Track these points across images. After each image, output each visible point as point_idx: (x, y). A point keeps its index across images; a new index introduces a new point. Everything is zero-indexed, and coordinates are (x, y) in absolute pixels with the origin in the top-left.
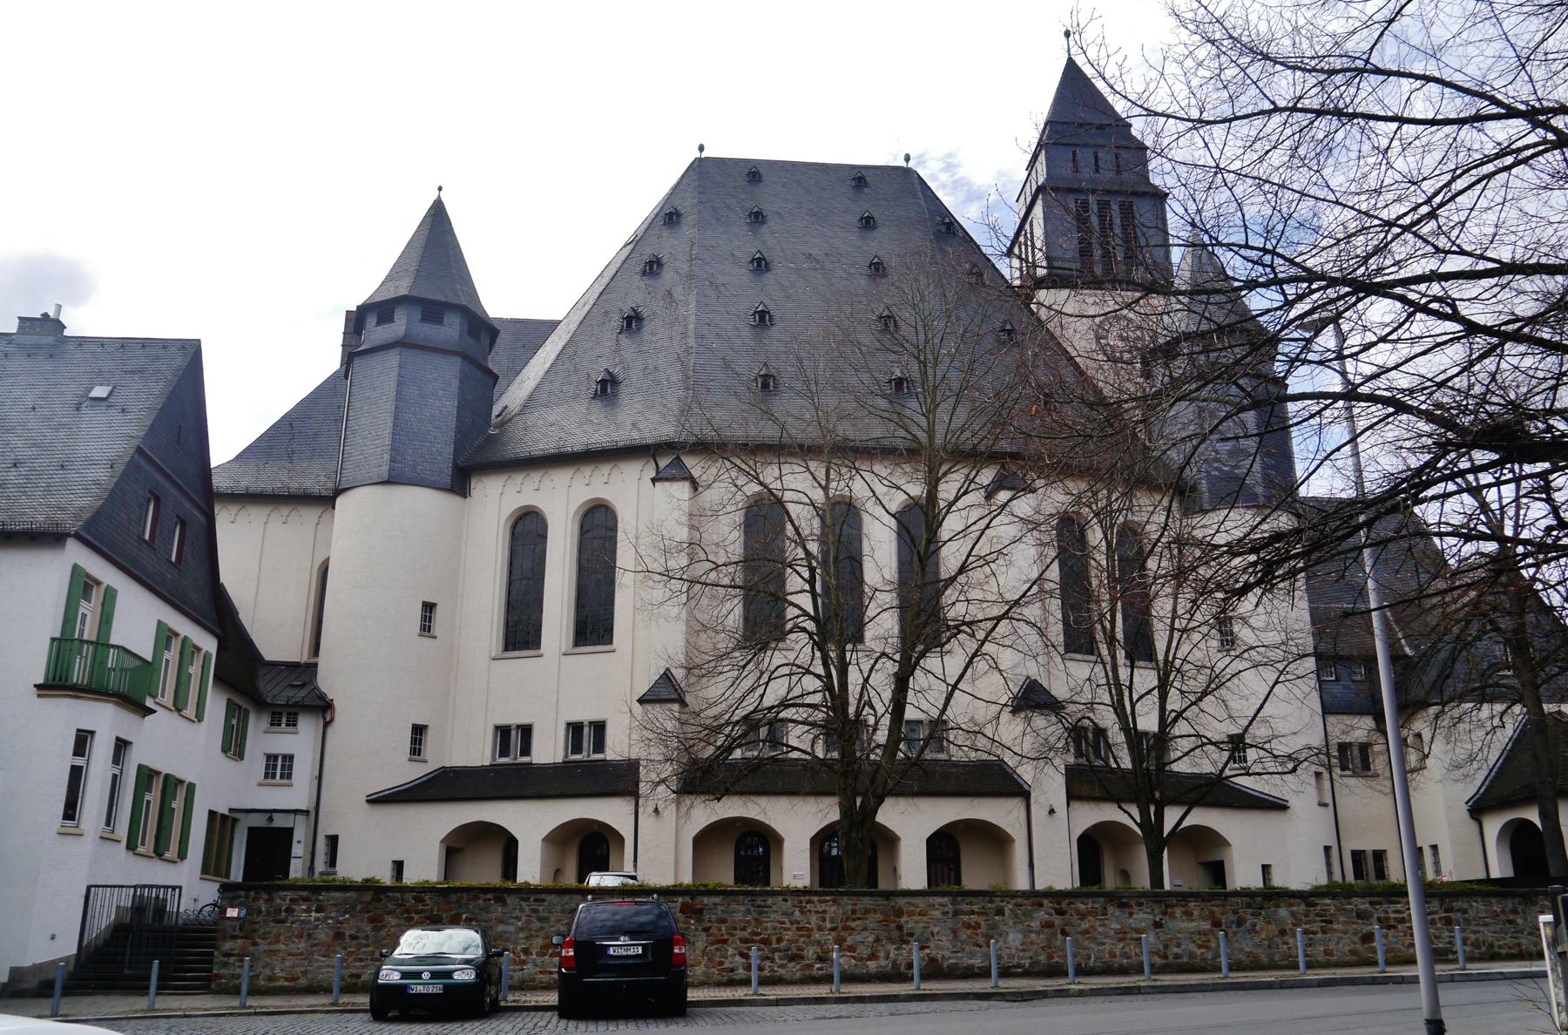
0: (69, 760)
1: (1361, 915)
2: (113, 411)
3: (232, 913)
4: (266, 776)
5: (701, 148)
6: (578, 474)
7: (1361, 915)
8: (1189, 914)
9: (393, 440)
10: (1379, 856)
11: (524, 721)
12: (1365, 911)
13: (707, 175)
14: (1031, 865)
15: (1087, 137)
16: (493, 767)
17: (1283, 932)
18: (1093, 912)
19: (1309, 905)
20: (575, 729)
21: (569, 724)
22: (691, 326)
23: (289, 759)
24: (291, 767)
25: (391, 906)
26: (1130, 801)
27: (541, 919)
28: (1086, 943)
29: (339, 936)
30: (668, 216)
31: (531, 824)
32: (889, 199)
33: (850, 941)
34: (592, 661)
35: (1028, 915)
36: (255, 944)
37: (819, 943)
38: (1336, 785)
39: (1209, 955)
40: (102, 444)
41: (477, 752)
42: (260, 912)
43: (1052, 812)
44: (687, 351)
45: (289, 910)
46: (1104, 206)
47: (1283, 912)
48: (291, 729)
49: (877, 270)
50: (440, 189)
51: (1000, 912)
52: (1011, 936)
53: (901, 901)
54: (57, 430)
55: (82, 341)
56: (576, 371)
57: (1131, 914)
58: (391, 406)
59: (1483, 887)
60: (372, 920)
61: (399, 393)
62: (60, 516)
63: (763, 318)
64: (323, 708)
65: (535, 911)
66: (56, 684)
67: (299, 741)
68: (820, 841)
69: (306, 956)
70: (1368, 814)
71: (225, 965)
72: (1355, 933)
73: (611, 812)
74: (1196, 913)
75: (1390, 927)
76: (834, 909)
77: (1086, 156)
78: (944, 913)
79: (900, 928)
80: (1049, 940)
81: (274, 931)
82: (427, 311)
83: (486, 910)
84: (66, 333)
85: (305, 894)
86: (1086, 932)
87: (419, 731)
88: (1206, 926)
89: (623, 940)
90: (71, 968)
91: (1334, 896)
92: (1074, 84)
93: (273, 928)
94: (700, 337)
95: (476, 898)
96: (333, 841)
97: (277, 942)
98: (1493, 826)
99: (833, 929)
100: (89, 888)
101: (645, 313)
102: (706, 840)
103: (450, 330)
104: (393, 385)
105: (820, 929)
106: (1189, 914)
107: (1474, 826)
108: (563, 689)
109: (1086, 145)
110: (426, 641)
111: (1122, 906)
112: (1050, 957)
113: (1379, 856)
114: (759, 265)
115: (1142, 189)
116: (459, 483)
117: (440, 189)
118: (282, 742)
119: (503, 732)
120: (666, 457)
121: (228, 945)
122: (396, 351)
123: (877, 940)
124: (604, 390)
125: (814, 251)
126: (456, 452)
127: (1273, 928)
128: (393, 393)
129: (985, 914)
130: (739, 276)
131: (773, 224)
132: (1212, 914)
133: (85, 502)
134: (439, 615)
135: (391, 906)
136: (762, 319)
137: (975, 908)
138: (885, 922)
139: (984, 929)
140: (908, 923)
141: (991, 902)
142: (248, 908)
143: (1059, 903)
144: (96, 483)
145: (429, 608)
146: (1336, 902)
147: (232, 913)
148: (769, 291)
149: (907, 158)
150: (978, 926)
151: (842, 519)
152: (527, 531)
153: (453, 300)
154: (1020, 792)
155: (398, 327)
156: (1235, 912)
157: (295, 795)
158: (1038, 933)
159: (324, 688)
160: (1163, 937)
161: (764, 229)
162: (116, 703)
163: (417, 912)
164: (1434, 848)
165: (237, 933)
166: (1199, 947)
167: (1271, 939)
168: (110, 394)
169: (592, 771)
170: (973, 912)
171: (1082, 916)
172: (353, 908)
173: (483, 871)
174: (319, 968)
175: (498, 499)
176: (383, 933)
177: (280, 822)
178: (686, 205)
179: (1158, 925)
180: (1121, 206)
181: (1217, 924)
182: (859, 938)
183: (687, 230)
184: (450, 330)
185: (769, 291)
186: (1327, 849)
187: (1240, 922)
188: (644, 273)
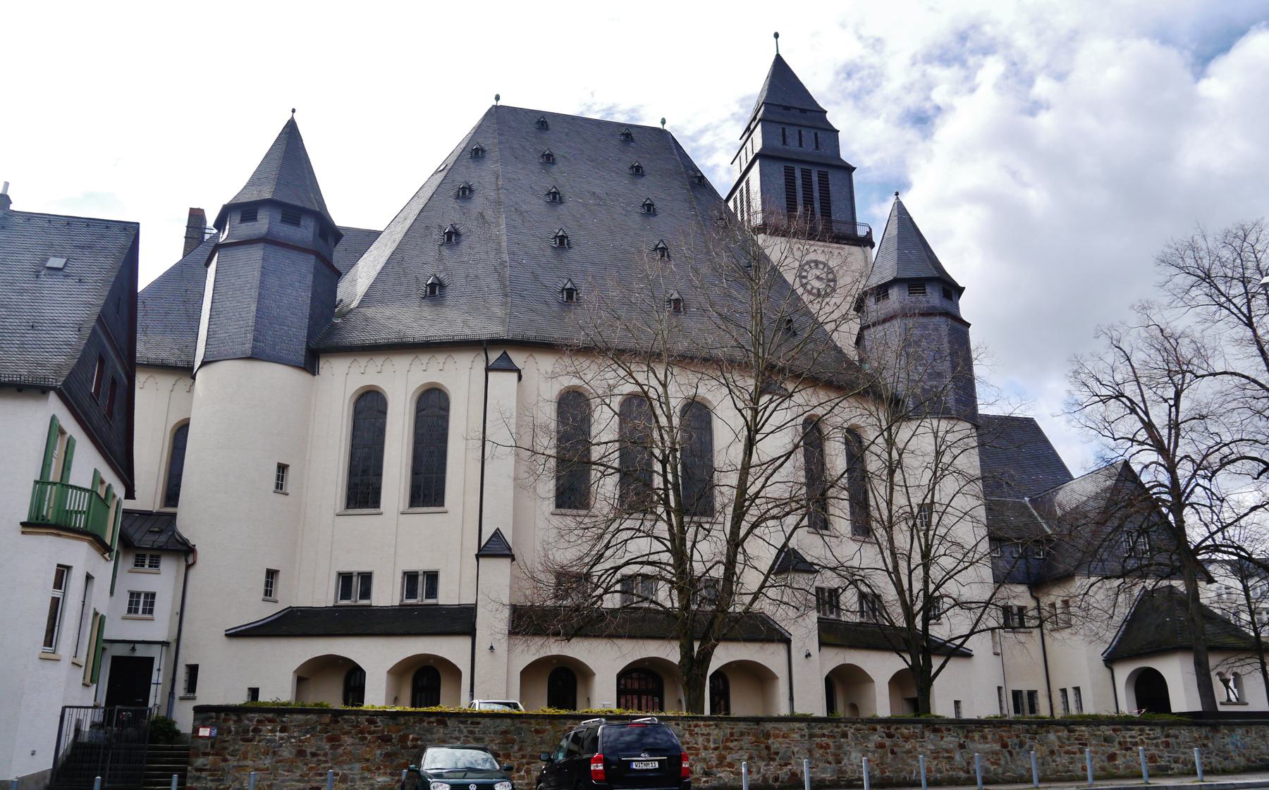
0: (52, 592)
1: (1107, 740)
2: (70, 281)
3: (204, 732)
4: (130, 611)
5: (497, 98)
6: (417, 362)
7: (1107, 740)
8: (984, 737)
9: (257, 323)
10: (1032, 694)
11: (365, 569)
12: (1110, 736)
13: (502, 119)
14: (791, 699)
15: (791, 119)
16: (336, 608)
17: (1052, 752)
18: (914, 736)
19: (1070, 731)
20: (411, 578)
21: (340, 574)
22: (504, 244)
23: (151, 596)
24: (152, 604)
25: (347, 727)
26: (904, 651)
28: (910, 761)
29: (301, 753)
30: (473, 151)
31: (378, 658)
32: (648, 154)
33: (729, 759)
34: (426, 520)
35: (866, 738)
36: (225, 760)
37: (704, 760)
38: (1046, 638)
39: (1000, 770)
40: (68, 311)
41: (323, 595)
42: (230, 732)
43: (808, 655)
44: (503, 264)
45: (256, 730)
47: (1052, 737)
48: (153, 570)
49: (649, 210)
50: (294, 111)
51: (845, 735)
52: (853, 755)
53: (769, 726)
54: (21, 294)
55: (29, 217)
56: (405, 275)
57: (942, 738)
58: (254, 293)
59: (1184, 719)
60: (330, 739)
61: (262, 282)
62: (41, 372)
63: (562, 242)
64: (185, 551)
65: (471, 732)
66: (35, 524)
67: (162, 580)
69: (272, 771)
71: (198, 779)
72: (1103, 754)
74: (990, 737)
75: (1127, 749)
76: (716, 732)
77: (792, 132)
78: (803, 736)
79: (768, 748)
80: (881, 758)
81: (243, 749)
82: (283, 209)
84: (12, 207)
85: (270, 716)
86: (909, 752)
87: (271, 574)
88: (997, 747)
89: (644, 756)
90: (47, 781)
91: (1087, 724)
92: (781, 73)
93: (241, 746)
94: (511, 253)
95: (421, 721)
96: (193, 670)
97: (245, 758)
98: (1123, 672)
99: (716, 749)
100: (64, 708)
101: (462, 230)
102: (529, 674)
103: (305, 232)
104: (257, 274)
105: (706, 748)
106: (984, 737)
107: (1107, 672)
108: (392, 545)
110: (280, 497)
111: (936, 731)
112: (883, 772)
113: (1032, 694)
114: (554, 198)
115: (834, 163)
116: (310, 364)
117: (294, 111)
118: (145, 581)
119: (345, 579)
120: (500, 351)
121: (200, 762)
122: (261, 245)
123: (751, 758)
124: (433, 292)
125: (598, 191)
126: (310, 337)
127: (1045, 749)
128: (256, 282)
129: (833, 737)
130: (538, 205)
131: (560, 165)
132: (1001, 737)
133: (61, 360)
134: (291, 474)
135: (347, 727)
136: (562, 243)
137: (826, 732)
138: (756, 743)
139: (832, 750)
140: (775, 744)
141: (838, 727)
143: (889, 728)
144: (67, 344)
145: (282, 468)
146: (1089, 729)
147: (204, 732)
149: (663, 122)
150: (828, 746)
151: (698, 413)
153: (308, 206)
155: (262, 224)
156: (1018, 736)
157: (158, 628)
158: (873, 752)
159: (185, 536)
160: (966, 756)
161: (554, 169)
162: (91, 543)
163: (370, 733)
164: (1077, 689)
165: (208, 750)
166: (993, 764)
167: (1043, 758)
168: (65, 264)
169: (426, 611)
170: (824, 735)
171: (906, 739)
172: (314, 729)
173: (332, 697)
174: (283, 781)
175: (342, 379)
176: (340, 751)
177: (141, 652)
178: (486, 143)
179: (962, 746)
180: (803, 171)
181: (1005, 746)
182: (736, 756)
183: (491, 165)
184: (305, 232)
186: (999, 688)
187: (1021, 745)
188: (458, 197)
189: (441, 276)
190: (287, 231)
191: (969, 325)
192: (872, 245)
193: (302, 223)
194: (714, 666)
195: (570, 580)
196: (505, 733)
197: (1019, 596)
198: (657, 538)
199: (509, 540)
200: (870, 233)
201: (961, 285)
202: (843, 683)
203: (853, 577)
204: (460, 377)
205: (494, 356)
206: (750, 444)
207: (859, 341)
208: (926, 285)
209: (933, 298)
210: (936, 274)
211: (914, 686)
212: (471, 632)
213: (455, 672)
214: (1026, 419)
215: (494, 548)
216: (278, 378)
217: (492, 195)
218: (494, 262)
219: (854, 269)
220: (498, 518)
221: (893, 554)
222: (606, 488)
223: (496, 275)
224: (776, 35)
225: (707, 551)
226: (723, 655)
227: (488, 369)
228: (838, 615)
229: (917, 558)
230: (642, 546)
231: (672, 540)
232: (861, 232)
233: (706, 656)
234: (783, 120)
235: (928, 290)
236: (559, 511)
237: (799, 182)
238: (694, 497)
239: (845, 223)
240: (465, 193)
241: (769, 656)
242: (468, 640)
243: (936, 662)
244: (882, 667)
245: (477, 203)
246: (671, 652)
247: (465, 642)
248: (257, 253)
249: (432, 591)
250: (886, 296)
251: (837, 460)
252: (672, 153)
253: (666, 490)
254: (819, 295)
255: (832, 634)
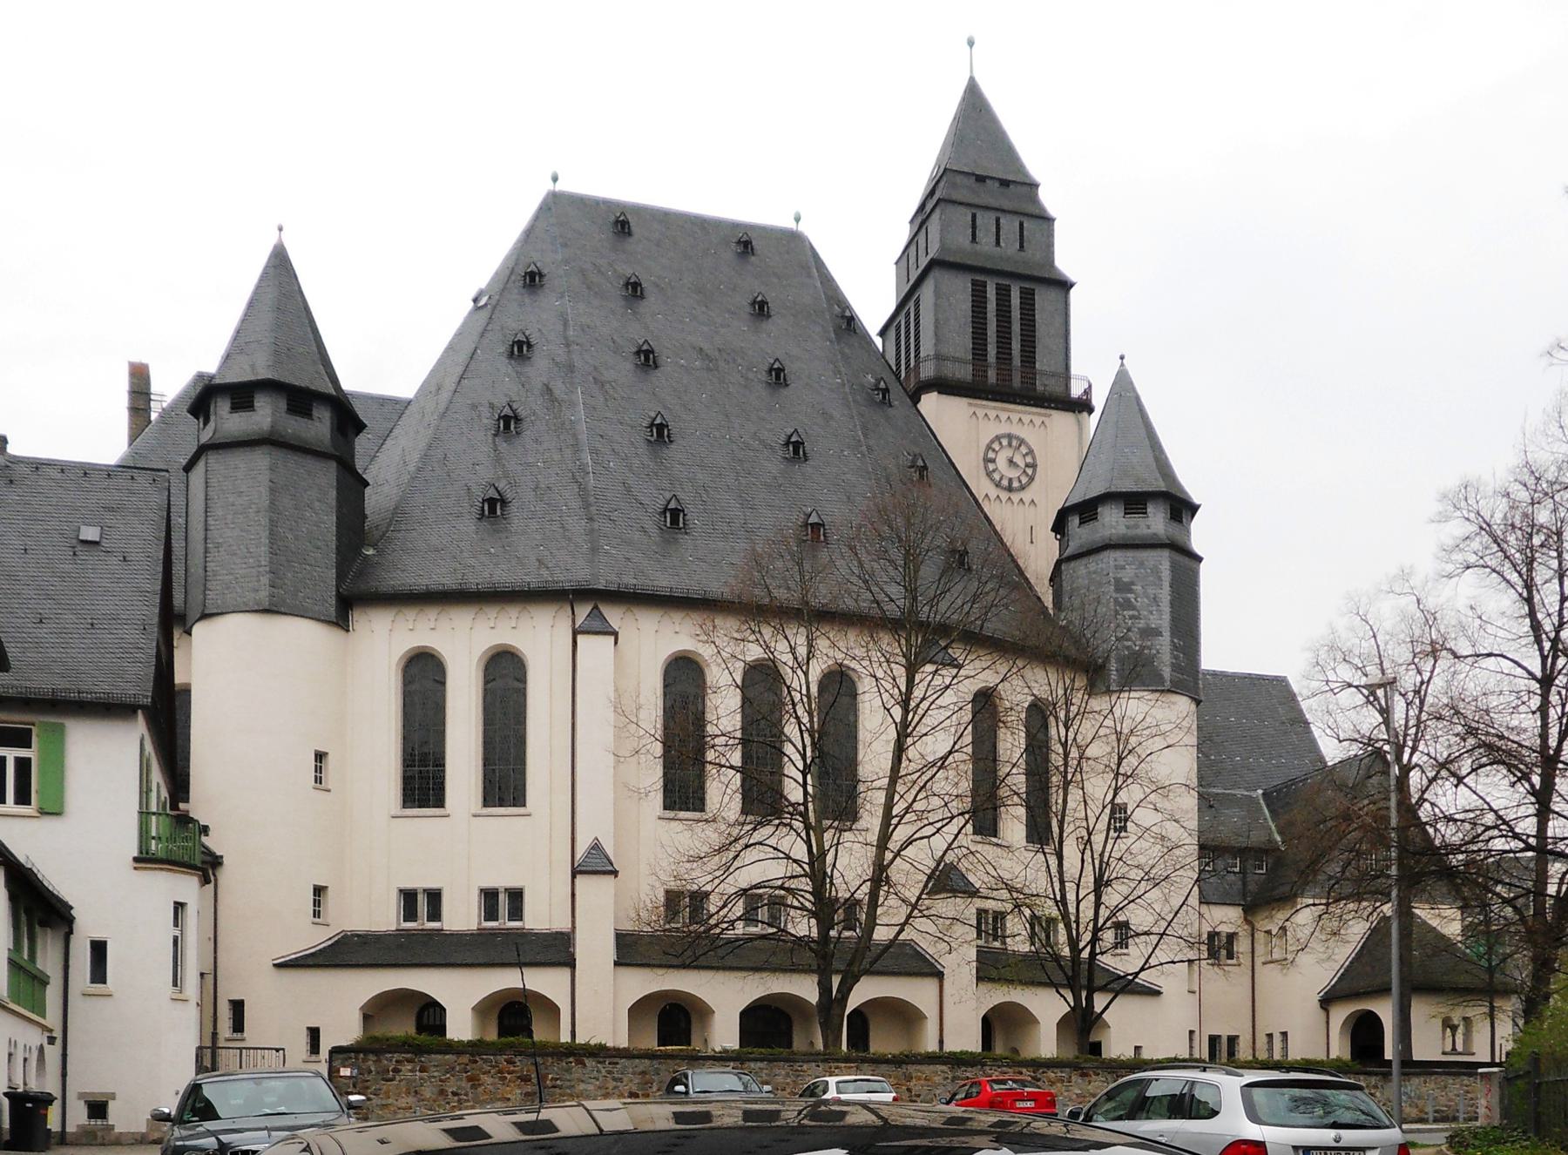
5: (555, 179)
14: (64, 1075)
16: (400, 933)
20: (490, 897)
22: (583, 437)
26: (1064, 986)
27: (614, 1079)
29: (442, 1092)
32: (764, 268)
34: (503, 822)
41: (385, 917)
42: (370, 1072)
46: (1003, 294)
55: (38, 465)
60: (470, 1079)
61: (272, 503)
63: (660, 433)
65: (609, 1072)
68: (1063, 1024)
70: (1225, 994)
73: (546, 982)
77: (986, 221)
79: (909, 1090)
83: (568, 1070)
93: (385, 1086)
94: (594, 452)
96: (238, 1007)
101: (522, 412)
102: (638, 1010)
103: (320, 427)
107: (1322, 1014)
108: (466, 853)
109: (987, 208)
111: (1083, 1075)
113: (1232, 1040)
116: (341, 620)
120: (592, 601)
122: (266, 449)
130: (623, 370)
134: (331, 763)
142: (359, 1068)
148: (663, 394)
152: (423, 673)
154: (929, 969)
155: (265, 414)
164: (1285, 1034)
175: (385, 638)
176: (480, 1089)
178: (546, 261)
180: (999, 288)
185: (663, 394)
186: (1191, 1032)
189: (501, 485)
190: (295, 427)
191: (1200, 559)
192: (1091, 410)
193: (315, 413)
194: (853, 1002)
195: (684, 903)
196: (643, 1073)
197: (1227, 918)
198: (795, 861)
199: (610, 851)
200: (1088, 392)
201: (1196, 501)
202: (1001, 1024)
203: (1021, 899)
204: (539, 637)
205: (583, 611)
206: (900, 750)
207: (1056, 576)
208: (1143, 509)
209: (1156, 521)
210: (1161, 486)
211: (1082, 1026)
212: (570, 963)
213: (552, 1009)
214: (1276, 678)
215: (593, 864)
216: (301, 636)
217: (561, 353)
218: (570, 466)
219: (1060, 455)
220: (595, 827)
221: (1062, 882)
222: (723, 791)
223: (575, 486)
224: (971, 43)
225: (850, 865)
226: (865, 991)
227: (575, 633)
228: (1004, 943)
229: (1089, 880)
230: (771, 860)
231: (811, 864)
232: (1076, 391)
233: (846, 990)
234: (976, 201)
235: (1150, 509)
236: (671, 814)
237: (992, 306)
238: (837, 795)
239: (1053, 375)
240: (520, 349)
241: (918, 993)
242: (566, 972)
243: (1100, 1001)
244: (1048, 1007)
245: (540, 367)
246: (806, 989)
247: (563, 975)
248: (261, 460)
249: (516, 912)
250: (1094, 517)
251: (1012, 745)
252: (809, 276)
253: (805, 804)
254: (1010, 489)
255: (992, 967)
